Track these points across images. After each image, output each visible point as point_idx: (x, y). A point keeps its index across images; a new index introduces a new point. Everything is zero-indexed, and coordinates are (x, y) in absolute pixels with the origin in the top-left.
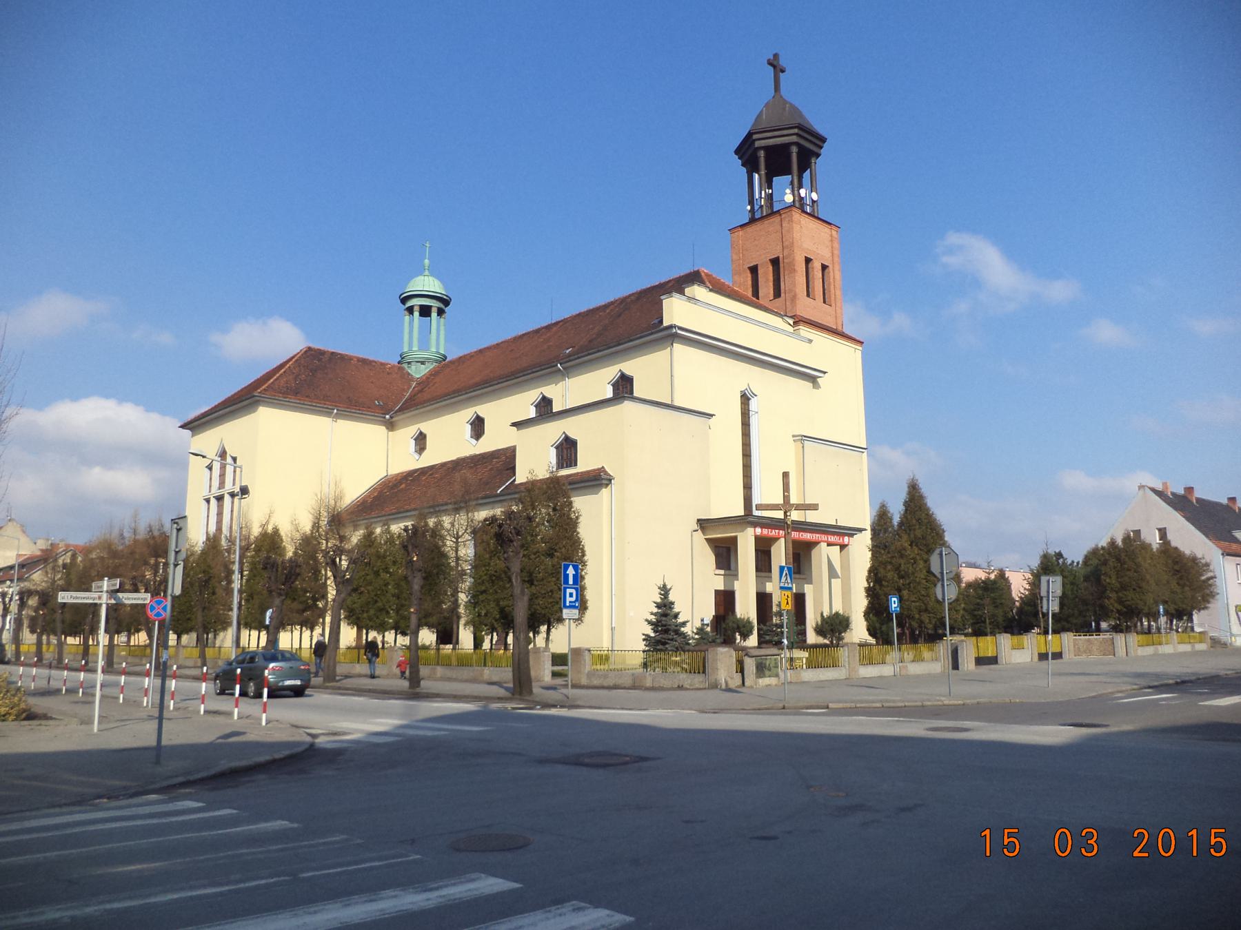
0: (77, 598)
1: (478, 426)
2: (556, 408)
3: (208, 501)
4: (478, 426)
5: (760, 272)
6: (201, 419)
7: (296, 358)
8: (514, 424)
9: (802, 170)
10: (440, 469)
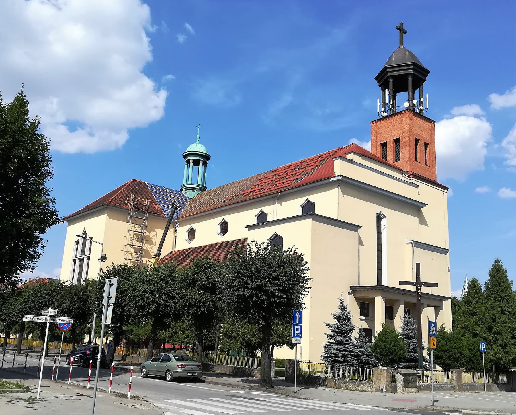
0: (34, 319)
1: (224, 227)
2: (269, 219)
3: (75, 261)
4: (224, 227)
5: (388, 146)
6: (73, 216)
7: (127, 185)
8: (246, 227)
9: (414, 89)
10: (202, 249)
